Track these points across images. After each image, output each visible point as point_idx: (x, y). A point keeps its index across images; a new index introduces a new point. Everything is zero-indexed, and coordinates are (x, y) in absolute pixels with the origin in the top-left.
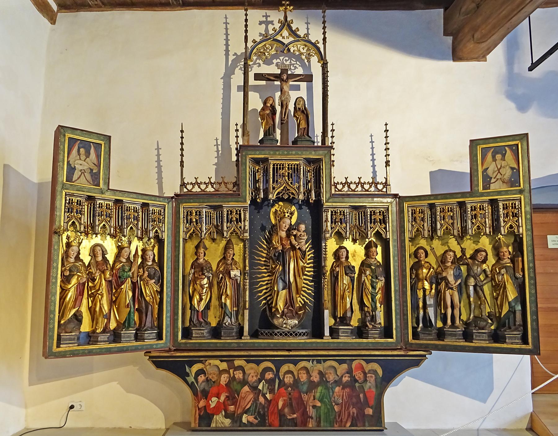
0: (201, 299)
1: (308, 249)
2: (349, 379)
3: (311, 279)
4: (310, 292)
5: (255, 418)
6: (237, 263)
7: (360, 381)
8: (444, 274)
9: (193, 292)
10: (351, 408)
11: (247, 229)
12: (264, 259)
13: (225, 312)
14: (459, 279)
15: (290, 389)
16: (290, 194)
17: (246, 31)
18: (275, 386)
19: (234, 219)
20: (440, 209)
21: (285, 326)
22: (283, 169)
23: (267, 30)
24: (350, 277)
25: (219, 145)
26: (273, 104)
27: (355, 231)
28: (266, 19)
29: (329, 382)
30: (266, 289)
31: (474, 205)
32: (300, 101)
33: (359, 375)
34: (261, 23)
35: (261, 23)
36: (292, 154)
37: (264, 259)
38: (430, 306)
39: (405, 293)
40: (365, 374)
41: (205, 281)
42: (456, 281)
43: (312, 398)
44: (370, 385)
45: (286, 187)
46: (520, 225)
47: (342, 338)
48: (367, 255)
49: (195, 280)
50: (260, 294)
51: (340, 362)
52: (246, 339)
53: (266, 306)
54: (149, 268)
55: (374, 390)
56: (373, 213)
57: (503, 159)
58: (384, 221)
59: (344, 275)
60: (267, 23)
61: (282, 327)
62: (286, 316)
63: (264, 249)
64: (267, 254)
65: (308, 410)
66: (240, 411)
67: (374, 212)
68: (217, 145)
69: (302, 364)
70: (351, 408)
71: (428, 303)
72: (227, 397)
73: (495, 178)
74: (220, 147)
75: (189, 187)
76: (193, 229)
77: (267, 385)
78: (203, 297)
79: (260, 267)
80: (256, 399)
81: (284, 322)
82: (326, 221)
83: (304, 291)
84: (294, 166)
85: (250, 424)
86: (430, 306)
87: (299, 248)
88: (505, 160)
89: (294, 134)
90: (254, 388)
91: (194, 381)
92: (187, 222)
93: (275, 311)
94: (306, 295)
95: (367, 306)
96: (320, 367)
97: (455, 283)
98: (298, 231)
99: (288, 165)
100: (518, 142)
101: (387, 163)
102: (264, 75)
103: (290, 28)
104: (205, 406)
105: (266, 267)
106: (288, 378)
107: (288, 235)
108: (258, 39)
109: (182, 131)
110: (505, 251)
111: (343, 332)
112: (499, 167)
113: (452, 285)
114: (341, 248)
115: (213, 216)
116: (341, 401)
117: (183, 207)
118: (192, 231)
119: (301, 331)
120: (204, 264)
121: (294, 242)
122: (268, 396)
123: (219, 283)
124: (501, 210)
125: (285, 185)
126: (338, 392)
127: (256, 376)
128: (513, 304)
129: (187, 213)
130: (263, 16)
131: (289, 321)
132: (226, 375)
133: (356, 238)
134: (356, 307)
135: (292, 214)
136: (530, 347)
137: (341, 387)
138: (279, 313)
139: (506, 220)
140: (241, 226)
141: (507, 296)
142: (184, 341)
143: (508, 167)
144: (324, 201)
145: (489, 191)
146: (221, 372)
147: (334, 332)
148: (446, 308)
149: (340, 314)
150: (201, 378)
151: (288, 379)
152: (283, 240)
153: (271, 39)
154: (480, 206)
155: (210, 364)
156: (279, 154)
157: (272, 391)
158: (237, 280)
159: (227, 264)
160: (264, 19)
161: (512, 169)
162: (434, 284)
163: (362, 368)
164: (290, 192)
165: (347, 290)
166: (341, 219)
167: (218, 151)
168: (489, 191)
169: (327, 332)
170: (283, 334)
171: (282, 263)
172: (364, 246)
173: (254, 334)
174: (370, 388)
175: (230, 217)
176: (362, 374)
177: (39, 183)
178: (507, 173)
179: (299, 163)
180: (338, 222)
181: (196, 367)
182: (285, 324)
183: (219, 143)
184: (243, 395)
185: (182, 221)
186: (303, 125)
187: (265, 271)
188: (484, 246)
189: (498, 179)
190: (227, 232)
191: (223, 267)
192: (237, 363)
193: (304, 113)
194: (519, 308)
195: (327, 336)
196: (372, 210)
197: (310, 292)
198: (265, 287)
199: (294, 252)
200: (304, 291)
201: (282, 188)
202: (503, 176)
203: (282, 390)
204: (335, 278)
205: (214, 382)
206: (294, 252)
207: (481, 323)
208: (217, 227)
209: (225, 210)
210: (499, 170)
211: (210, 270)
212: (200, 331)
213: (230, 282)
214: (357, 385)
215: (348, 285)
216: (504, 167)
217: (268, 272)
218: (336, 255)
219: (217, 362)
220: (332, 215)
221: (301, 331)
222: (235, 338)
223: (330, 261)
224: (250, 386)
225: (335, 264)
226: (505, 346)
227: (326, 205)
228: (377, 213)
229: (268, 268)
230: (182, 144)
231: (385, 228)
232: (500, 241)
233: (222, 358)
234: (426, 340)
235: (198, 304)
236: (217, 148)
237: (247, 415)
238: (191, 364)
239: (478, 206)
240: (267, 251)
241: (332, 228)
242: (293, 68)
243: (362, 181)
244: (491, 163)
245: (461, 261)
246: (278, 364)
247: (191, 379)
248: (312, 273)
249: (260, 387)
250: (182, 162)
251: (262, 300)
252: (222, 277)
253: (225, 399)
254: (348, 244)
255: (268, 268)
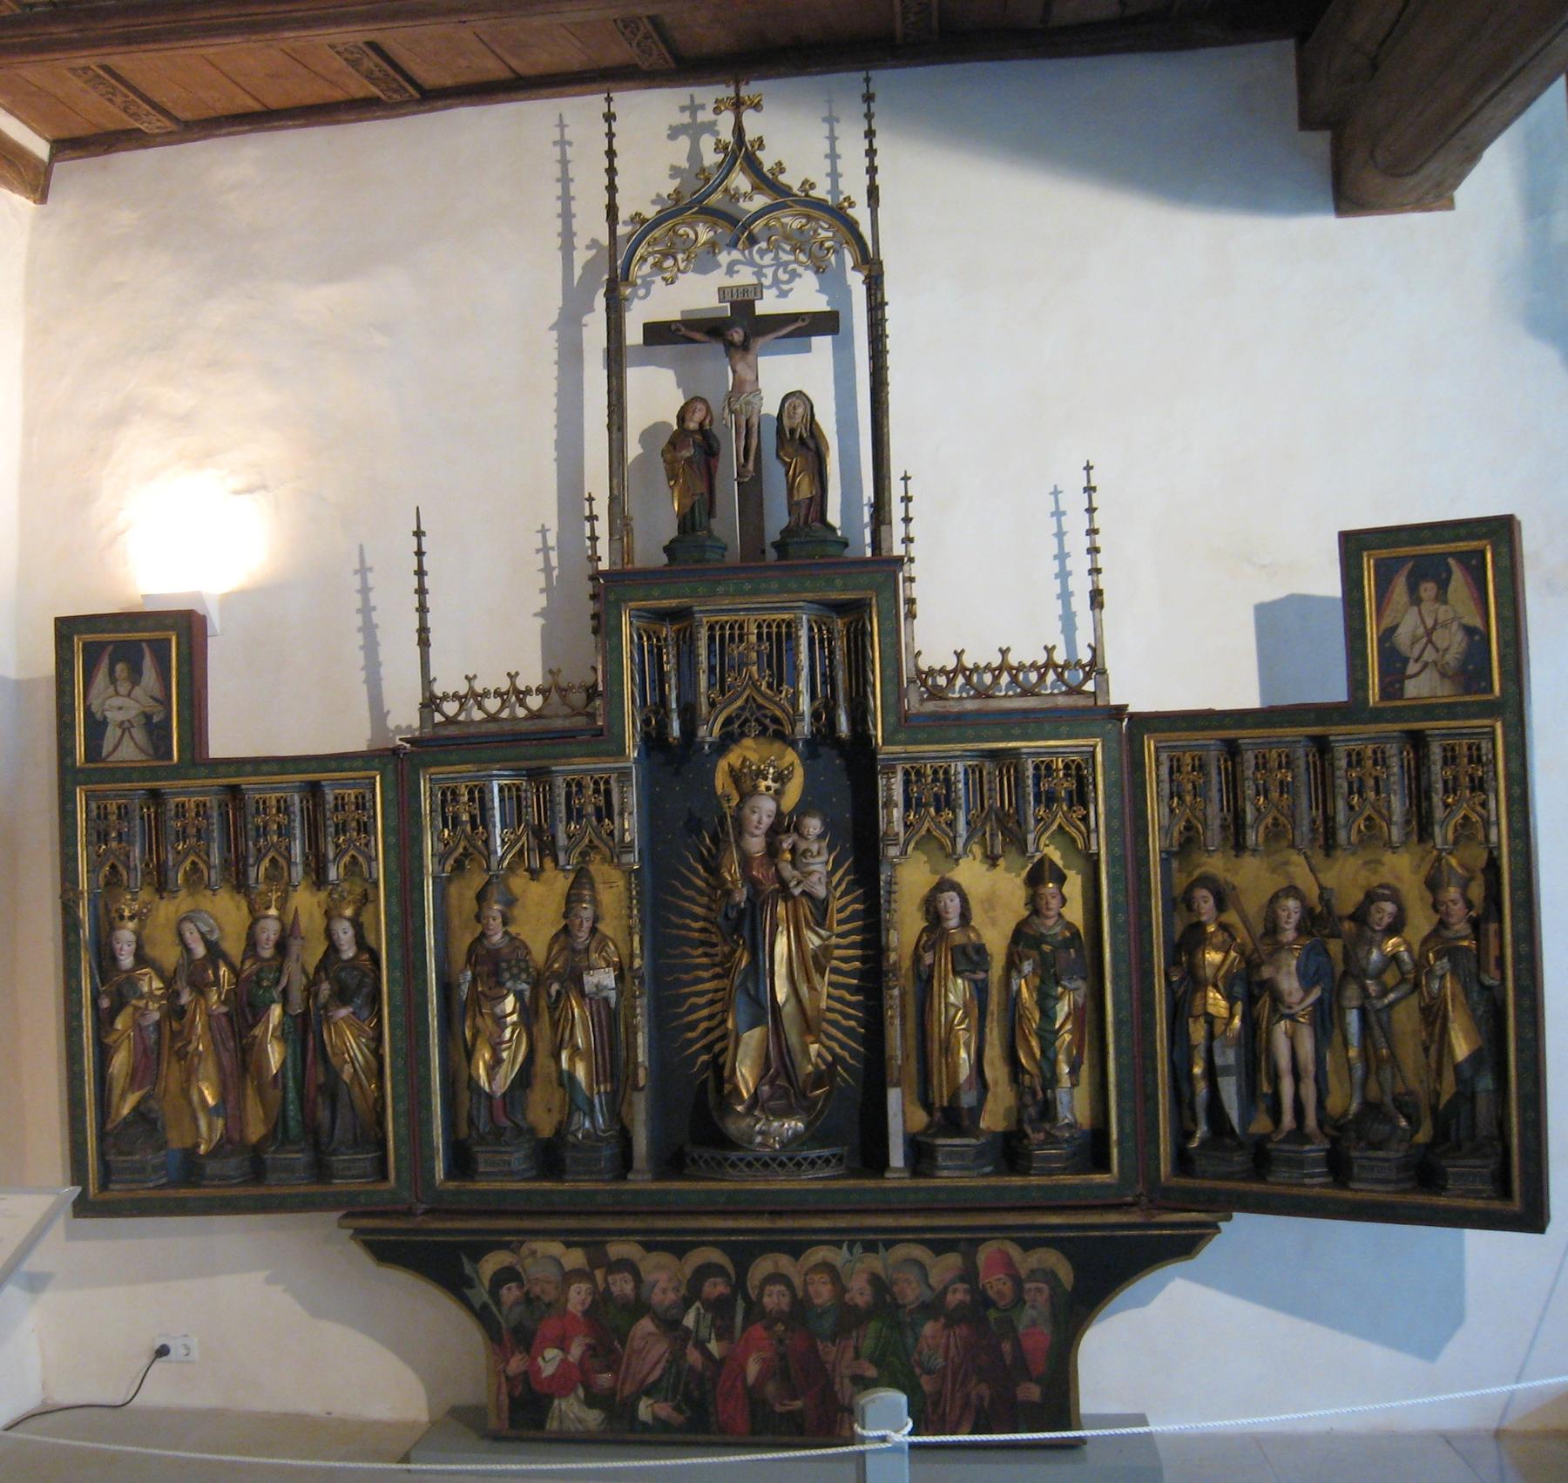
0: (497, 1061)
1: (843, 887)
2: (968, 1298)
3: (855, 982)
4: (852, 1023)
5: (677, 1409)
6: (607, 944)
7: (1001, 1304)
8: (1266, 972)
9: (475, 1038)
10: (973, 1383)
11: (632, 841)
12: (700, 924)
13: (572, 1100)
14: (1314, 985)
15: (780, 1327)
16: (767, 721)
17: (612, 188)
18: (733, 1318)
19: (590, 809)
20: (1256, 757)
21: (759, 1139)
22: (741, 640)
23: (695, 155)
24: (975, 982)
25: (553, 549)
26: (707, 421)
27: (992, 830)
28: (693, 115)
29: (904, 1306)
30: (711, 1017)
31: (1357, 748)
32: (795, 408)
33: (996, 1284)
34: (674, 133)
35: (674, 133)
36: (768, 592)
37: (700, 924)
38: (1227, 1070)
39: (1148, 1027)
40: (1018, 1282)
41: (509, 1003)
42: (1307, 992)
43: (850, 1354)
44: (1034, 1319)
45: (754, 700)
46: (1493, 818)
47: (945, 1173)
48: (1035, 905)
49: (476, 1000)
50: (690, 1035)
51: (939, 1248)
52: (641, 1181)
53: (708, 1074)
54: (343, 969)
55: (1046, 1329)
56: (1043, 772)
57: (1442, 597)
58: (1080, 797)
59: (951, 976)
60: (694, 131)
61: (751, 1142)
62: (763, 1110)
63: (700, 891)
64: (709, 908)
65: (837, 1387)
66: (628, 1389)
67: (1048, 767)
68: (545, 549)
69: (820, 1254)
70: (973, 1383)
71: (1219, 1061)
72: (589, 1347)
73: (1417, 660)
74: (554, 556)
75: (451, 708)
76: (462, 844)
77: (709, 1316)
78: (505, 1055)
79: (688, 950)
80: (677, 1356)
81: (758, 1127)
82: (886, 805)
83: (834, 1023)
84: (779, 626)
85: (661, 1425)
86: (1227, 1070)
87: (804, 893)
88: (1445, 602)
89: (777, 519)
90: (670, 1324)
91: (490, 1302)
92: (445, 825)
93: (730, 1093)
94: (840, 1035)
95: (1028, 1073)
96: (875, 1262)
97: (1302, 1000)
98: (801, 836)
99: (759, 627)
100: (1485, 542)
101: (1096, 598)
102: (673, 327)
103: (753, 166)
104: (526, 1373)
105: (709, 950)
106: (775, 1297)
107: (772, 851)
108: (650, 212)
109: (419, 534)
110: (1452, 901)
111: (950, 1155)
112: (1430, 623)
113: (1290, 1008)
114: (945, 885)
115: (526, 798)
116: (940, 1362)
117: (431, 779)
118: (461, 850)
119: (813, 1154)
120: (506, 951)
121: (788, 871)
122: (713, 1346)
123: (553, 1007)
124: (1437, 768)
125: (747, 692)
126: (933, 1337)
127: (676, 1289)
128: (1467, 1073)
129: (444, 794)
130: (683, 109)
131: (776, 1124)
132: (584, 1286)
133: (992, 851)
134: (996, 1071)
135: (781, 778)
136: (1516, 1205)
137: (942, 1320)
138: (741, 1100)
139: (1450, 800)
140: (612, 831)
141: (1450, 1045)
142: (452, 1185)
143: (1455, 627)
144: (880, 741)
145: (1399, 703)
146: (569, 1277)
147: (920, 1153)
148: (1275, 1079)
149: (941, 1096)
150: (510, 1293)
151: (775, 1299)
152: (755, 865)
153: (691, 208)
154: (1375, 752)
155: (533, 1253)
156: (726, 594)
157: (724, 1333)
158: (606, 999)
159: (574, 951)
160: (685, 118)
161: (1469, 631)
162: (1239, 1003)
163: (1009, 1264)
164: (765, 716)
165: (959, 1024)
166: (937, 797)
167: (547, 569)
168: (1399, 703)
169: (897, 1157)
170: (758, 1165)
171: (748, 941)
172: (1024, 873)
173: (672, 1163)
174: (1034, 1323)
175: (576, 802)
176: (1009, 1284)
177: (19, 684)
178: (1453, 643)
179: (792, 616)
180: (926, 805)
181: (492, 1263)
182: (761, 1133)
183: (552, 540)
184: (637, 1344)
185: (427, 822)
186: (805, 490)
187: (704, 960)
188: (1397, 878)
189: (1426, 665)
190: (568, 851)
191: (562, 959)
192: (618, 1250)
193: (808, 448)
194: (1486, 1083)
195: (897, 1170)
196: (1042, 762)
197: (852, 1023)
198: (705, 1012)
199: (790, 904)
200: (834, 1023)
201: (740, 703)
202: (1443, 656)
203: (757, 1330)
204: (925, 983)
205: (549, 1305)
206: (790, 904)
207: (1375, 1126)
208: (537, 832)
209: (560, 782)
210: (1429, 633)
211: (521, 970)
212: (498, 1157)
213: (581, 1007)
214: (992, 1314)
215: (965, 1007)
216: (1445, 625)
217: (714, 965)
218: (932, 910)
219: (555, 1248)
220: (907, 783)
221: (813, 1154)
222: (607, 1177)
223: (905, 929)
224: (656, 1318)
225: (925, 938)
226: (1442, 1201)
227: (885, 751)
228: (1057, 770)
229: (712, 951)
230: (420, 573)
231: (1085, 819)
232: (1440, 864)
233: (569, 1239)
234: (1215, 1177)
235: (488, 1075)
236: (547, 559)
237: (651, 1402)
238: (478, 1251)
239: (1369, 752)
240: (709, 896)
241: (907, 826)
242: (785, 277)
243: (1013, 660)
244: (1406, 612)
245: (1326, 928)
246: (743, 1254)
247: (481, 1295)
248: (857, 964)
249: (689, 1321)
250: (423, 631)
251: (697, 1054)
252: (558, 993)
253: (583, 1353)
254: (970, 872)
255: (712, 951)
